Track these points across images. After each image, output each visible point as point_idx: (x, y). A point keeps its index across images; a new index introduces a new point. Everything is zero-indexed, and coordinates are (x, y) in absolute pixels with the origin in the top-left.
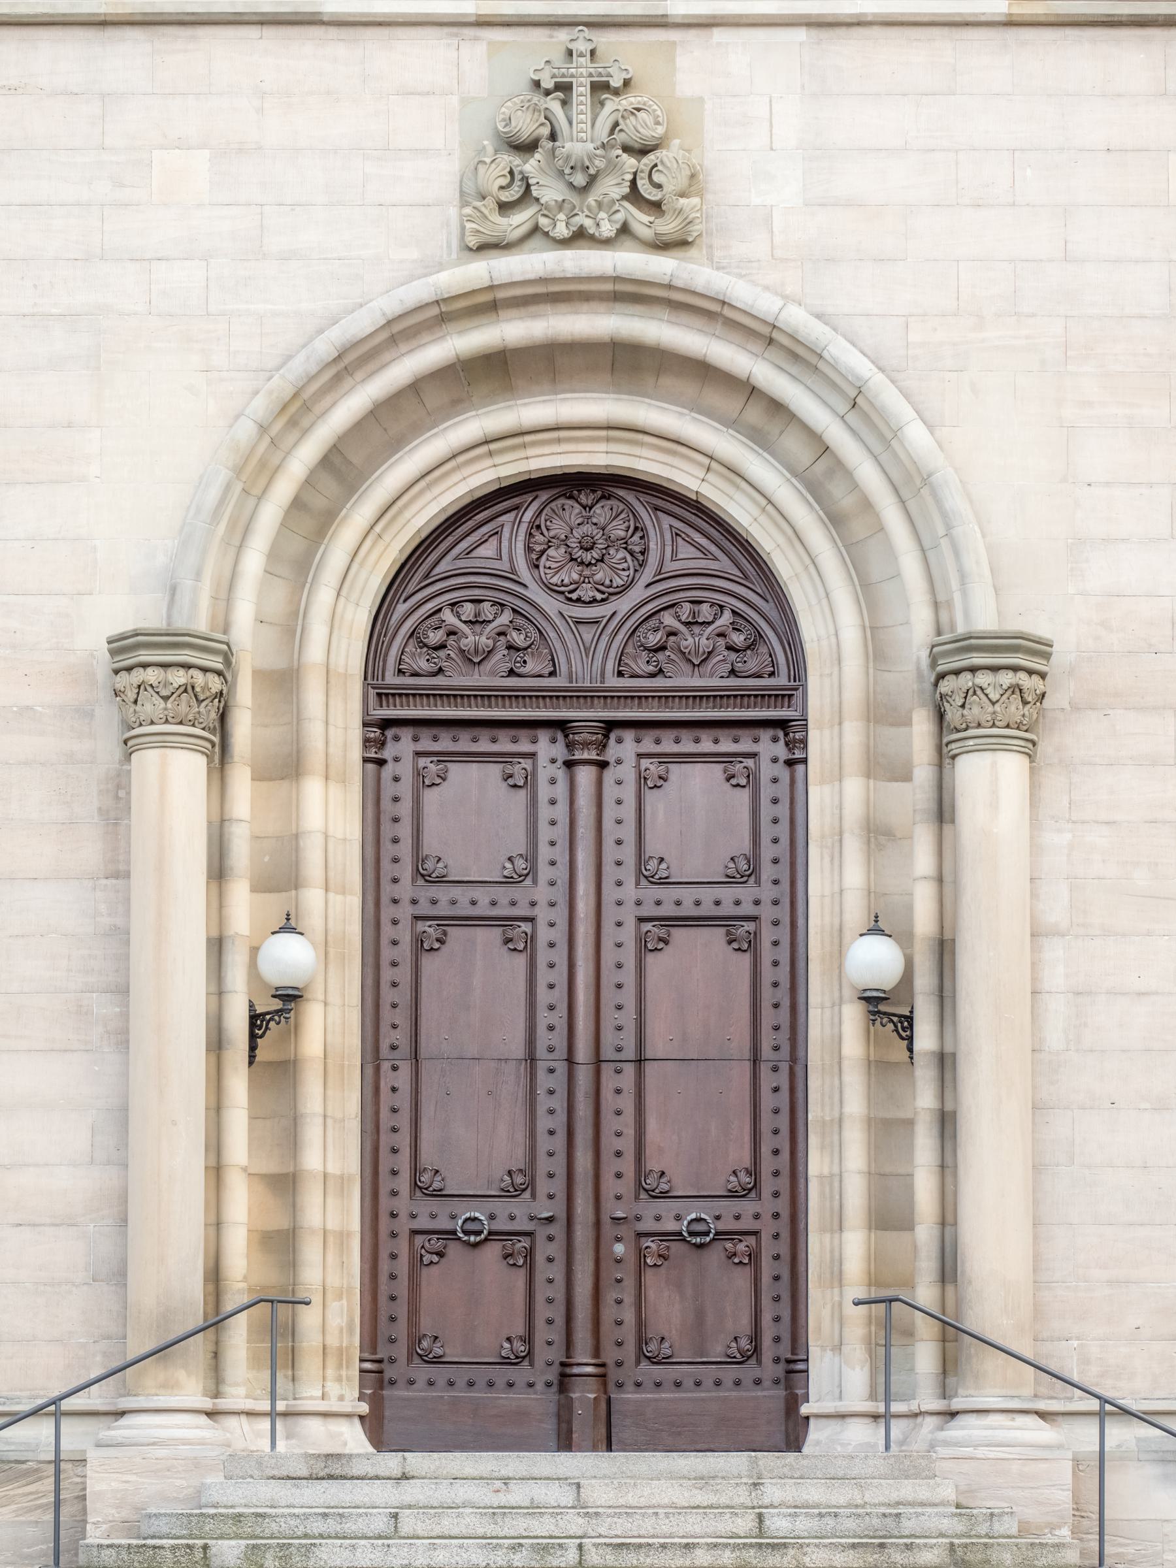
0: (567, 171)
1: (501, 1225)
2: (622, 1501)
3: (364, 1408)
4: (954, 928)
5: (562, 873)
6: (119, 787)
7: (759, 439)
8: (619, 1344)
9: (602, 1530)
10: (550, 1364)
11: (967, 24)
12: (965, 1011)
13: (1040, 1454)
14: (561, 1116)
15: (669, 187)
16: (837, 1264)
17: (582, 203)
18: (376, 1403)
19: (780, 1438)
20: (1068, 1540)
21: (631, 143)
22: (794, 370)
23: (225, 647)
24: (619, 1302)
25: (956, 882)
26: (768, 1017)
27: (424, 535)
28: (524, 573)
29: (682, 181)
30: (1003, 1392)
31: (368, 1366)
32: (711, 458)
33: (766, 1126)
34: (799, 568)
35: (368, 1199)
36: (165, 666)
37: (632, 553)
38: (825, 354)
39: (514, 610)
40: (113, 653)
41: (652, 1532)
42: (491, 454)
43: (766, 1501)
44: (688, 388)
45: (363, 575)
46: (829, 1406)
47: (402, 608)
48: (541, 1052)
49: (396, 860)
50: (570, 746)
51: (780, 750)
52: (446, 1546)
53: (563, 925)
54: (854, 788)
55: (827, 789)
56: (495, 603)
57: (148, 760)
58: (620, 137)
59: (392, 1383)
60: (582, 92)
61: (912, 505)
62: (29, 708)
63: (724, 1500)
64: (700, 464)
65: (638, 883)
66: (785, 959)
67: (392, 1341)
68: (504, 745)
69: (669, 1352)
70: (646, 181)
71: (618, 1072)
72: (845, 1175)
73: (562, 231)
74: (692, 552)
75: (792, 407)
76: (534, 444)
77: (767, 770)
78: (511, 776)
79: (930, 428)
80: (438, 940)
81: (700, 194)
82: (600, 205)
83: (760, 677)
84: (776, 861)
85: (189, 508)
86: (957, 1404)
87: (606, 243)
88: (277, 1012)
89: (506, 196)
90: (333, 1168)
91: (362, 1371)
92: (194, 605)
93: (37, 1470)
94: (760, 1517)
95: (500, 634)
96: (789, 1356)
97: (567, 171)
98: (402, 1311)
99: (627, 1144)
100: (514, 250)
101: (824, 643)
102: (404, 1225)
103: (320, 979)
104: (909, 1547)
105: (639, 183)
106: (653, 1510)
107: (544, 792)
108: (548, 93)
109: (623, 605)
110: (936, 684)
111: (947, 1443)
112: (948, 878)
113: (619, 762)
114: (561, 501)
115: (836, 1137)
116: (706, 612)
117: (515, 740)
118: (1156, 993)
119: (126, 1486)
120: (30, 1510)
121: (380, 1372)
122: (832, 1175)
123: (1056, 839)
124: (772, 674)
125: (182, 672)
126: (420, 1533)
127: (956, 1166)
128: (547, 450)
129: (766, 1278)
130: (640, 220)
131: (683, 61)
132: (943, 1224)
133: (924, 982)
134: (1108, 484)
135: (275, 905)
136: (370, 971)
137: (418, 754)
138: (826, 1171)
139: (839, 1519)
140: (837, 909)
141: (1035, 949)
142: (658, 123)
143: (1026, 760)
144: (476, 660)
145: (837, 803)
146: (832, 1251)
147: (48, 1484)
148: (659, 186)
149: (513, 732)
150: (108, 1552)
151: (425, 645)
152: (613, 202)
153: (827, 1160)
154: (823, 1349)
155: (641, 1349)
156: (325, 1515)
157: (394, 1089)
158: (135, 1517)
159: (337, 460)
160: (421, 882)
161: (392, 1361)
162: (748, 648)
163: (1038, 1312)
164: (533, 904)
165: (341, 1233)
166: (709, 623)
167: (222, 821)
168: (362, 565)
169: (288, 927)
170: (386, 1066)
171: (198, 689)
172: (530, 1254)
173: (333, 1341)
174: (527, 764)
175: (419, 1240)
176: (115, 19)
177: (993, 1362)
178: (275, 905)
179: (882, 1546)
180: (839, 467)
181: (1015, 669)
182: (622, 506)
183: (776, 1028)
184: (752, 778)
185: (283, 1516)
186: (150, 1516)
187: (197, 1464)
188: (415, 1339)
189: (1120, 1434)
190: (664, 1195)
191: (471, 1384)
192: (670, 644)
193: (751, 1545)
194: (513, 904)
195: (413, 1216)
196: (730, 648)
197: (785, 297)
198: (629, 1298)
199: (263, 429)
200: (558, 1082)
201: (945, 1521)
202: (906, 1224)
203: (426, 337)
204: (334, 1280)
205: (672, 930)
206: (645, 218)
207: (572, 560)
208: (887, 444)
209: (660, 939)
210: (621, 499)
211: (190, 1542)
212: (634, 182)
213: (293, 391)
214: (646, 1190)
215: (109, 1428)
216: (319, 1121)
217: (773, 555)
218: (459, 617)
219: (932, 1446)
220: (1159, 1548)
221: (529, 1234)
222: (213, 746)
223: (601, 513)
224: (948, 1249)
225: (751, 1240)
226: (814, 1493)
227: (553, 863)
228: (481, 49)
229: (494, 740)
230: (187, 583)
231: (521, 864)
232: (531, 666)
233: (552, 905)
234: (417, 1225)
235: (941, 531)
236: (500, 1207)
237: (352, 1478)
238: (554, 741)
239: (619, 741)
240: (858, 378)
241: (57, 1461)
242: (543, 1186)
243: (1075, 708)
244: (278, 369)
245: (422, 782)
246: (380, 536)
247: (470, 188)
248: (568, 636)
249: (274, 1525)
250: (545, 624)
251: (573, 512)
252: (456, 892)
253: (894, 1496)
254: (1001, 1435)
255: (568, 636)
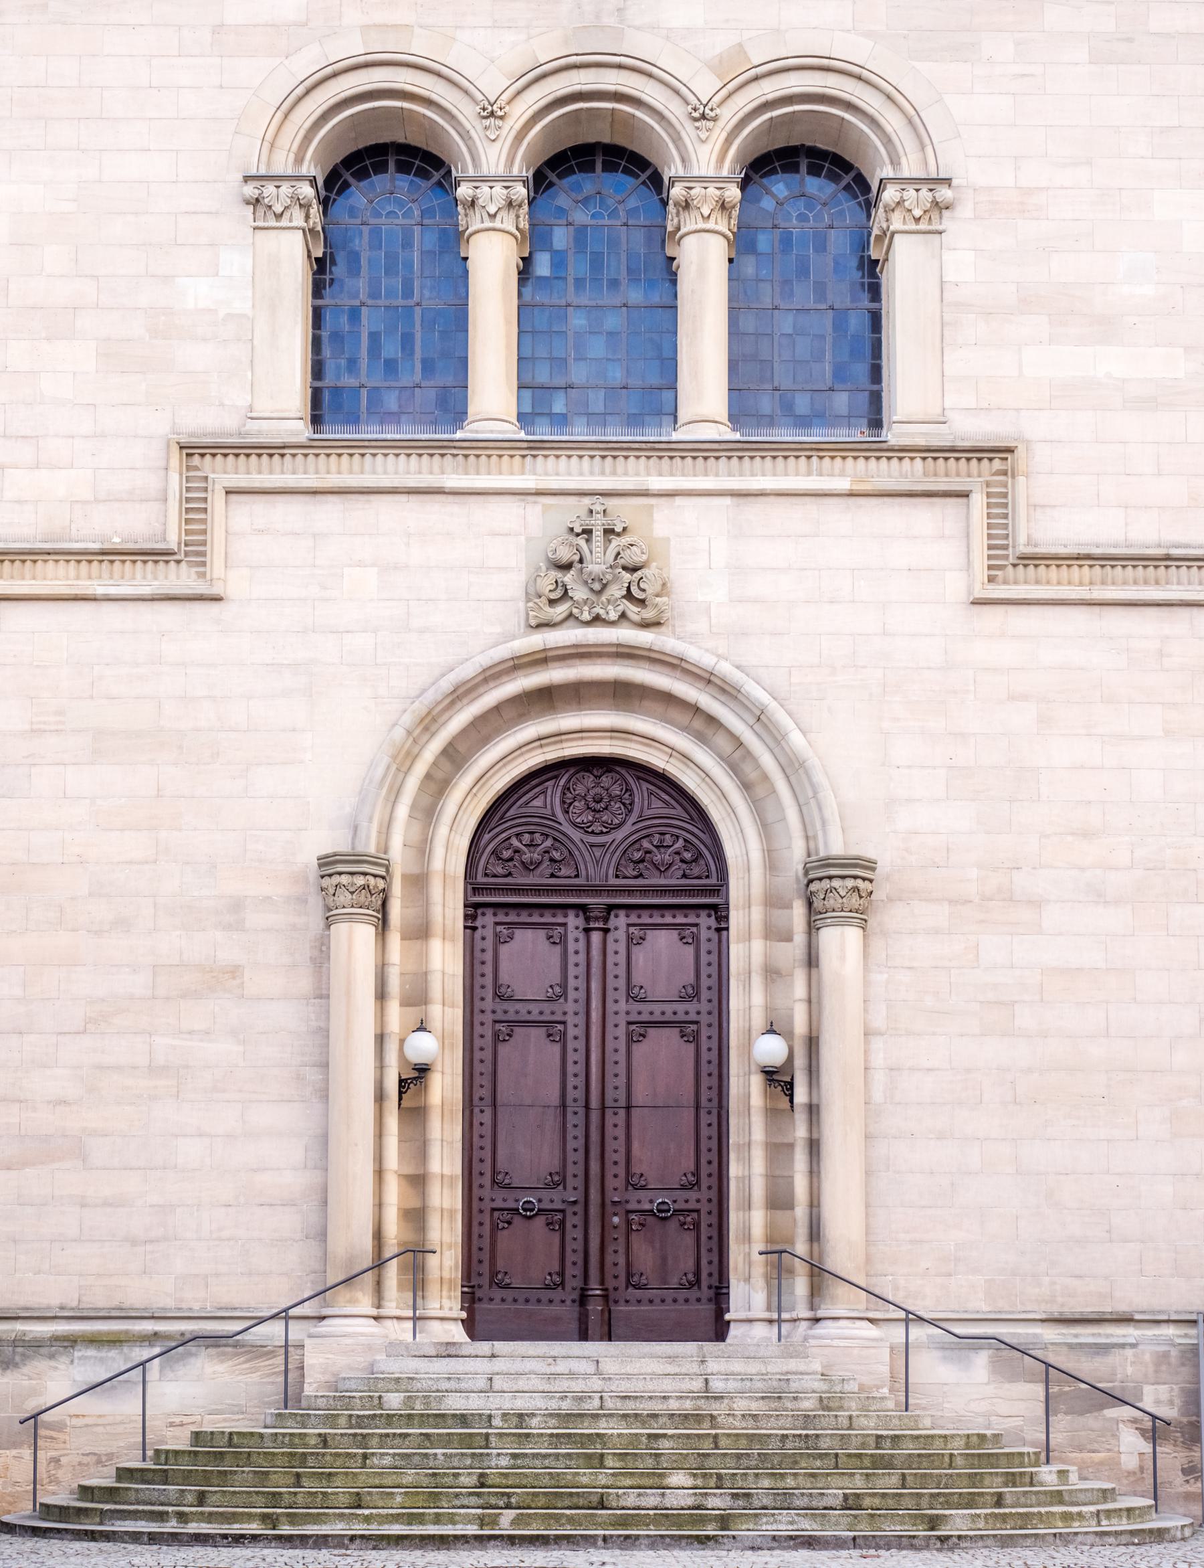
0: (590, 581)
1: (546, 1205)
2: (623, 1371)
3: (464, 1315)
4: (818, 1030)
5: (582, 995)
6: (322, 944)
7: (701, 738)
8: (616, 1277)
9: (613, 1388)
10: (574, 1289)
11: (826, 495)
12: (825, 1079)
13: (874, 1344)
14: (582, 1141)
15: (650, 591)
16: (747, 1230)
17: (598, 600)
18: (471, 1311)
19: (712, 1334)
20: (887, 1395)
21: (628, 565)
22: (723, 698)
23: (387, 862)
24: (616, 1252)
25: (819, 1003)
26: (705, 1082)
27: (500, 793)
28: (560, 816)
29: (658, 588)
30: (848, 1307)
31: (466, 1289)
32: (673, 749)
33: (703, 1148)
34: (725, 815)
35: (466, 1189)
36: (352, 874)
37: (624, 804)
38: (742, 690)
39: (554, 839)
40: (320, 866)
41: (642, 1389)
42: (541, 746)
43: (709, 1371)
44: (658, 707)
45: (465, 818)
46: (742, 1315)
47: (487, 837)
48: (569, 1102)
49: (483, 987)
50: (587, 919)
51: (712, 922)
52: (522, 1397)
53: (582, 1026)
54: (758, 946)
55: (741, 945)
56: (542, 834)
57: (341, 930)
58: (620, 561)
59: (480, 1300)
60: (598, 534)
61: (792, 779)
62: (269, 898)
63: (684, 1371)
64: (666, 753)
65: (627, 1001)
66: (715, 1046)
67: (480, 1275)
68: (548, 918)
69: (645, 1282)
70: (636, 587)
71: (616, 1114)
72: (752, 1177)
73: (586, 616)
74: (660, 804)
75: (722, 721)
76: (567, 740)
77: (704, 934)
78: (552, 937)
79: (804, 733)
80: (508, 1035)
81: (668, 595)
82: (609, 601)
83: (701, 878)
84: (709, 988)
85: (365, 779)
86: (820, 1314)
87: (612, 623)
88: (415, 1078)
89: (553, 596)
90: (447, 1171)
91: (463, 1293)
92: (368, 837)
93: (273, 1352)
94: (706, 1380)
95: (545, 852)
96: (717, 1284)
97: (590, 581)
98: (486, 1256)
99: (621, 1157)
100: (557, 628)
101: (740, 859)
102: (487, 1205)
103: (440, 1059)
104: (795, 1399)
105: (632, 588)
106: (643, 1376)
107: (571, 946)
108: (578, 535)
109: (619, 835)
110: (808, 885)
111: (814, 1337)
112: (814, 1000)
113: (616, 929)
114: (582, 774)
115: (747, 1154)
116: (668, 840)
117: (554, 916)
118: (938, 1069)
119: (327, 1361)
120: (269, 1375)
121: (473, 1293)
122: (744, 1177)
123: (879, 978)
124: (707, 877)
125: (362, 877)
126: (505, 1389)
127: (819, 1172)
128: (574, 743)
129: (703, 1238)
130: (633, 610)
131: (657, 516)
132: (811, 1206)
133: (800, 1062)
134: (909, 767)
135: (414, 1013)
136: (467, 1053)
137: (497, 924)
138: (740, 1174)
139: (753, 1382)
140: (747, 1017)
141: (867, 1042)
142: (643, 553)
143: (861, 930)
144: (532, 868)
145: (747, 954)
146: (744, 1222)
147: (280, 1360)
148: (644, 590)
149: (552, 911)
150: (321, 1400)
151: (501, 859)
152: (617, 600)
153: (741, 1167)
154: (739, 1280)
155: (629, 1280)
156: (449, 1379)
157: (481, 1124)
158: (333, 1380)
159: (451, 750)
160: (498, 1000)
161: (480, 1287)
162: (693, 861)
163: (868, 1259)
164: (565, 1013)
165: (451, 1211)
166: (670, 846)
167: (383, 965)
168: (464, 812)
169: (422, 1028)
170: (476, 1110)
171: (371, 887)
172: (563, 1223)
173: (446, 1275)
174: (560, 929)
175: (496, 1214)
176: (321, 490)
177: (842, 1290)
178: (414, 1013)
179: (779, 1398)
180: (749, 754)
181: (855, 877)
182: (618, 777)
183: (710, 1088)
184: (696, 939)
185: (424, 1379)
186: (344, 1379)
187: (370, 1348)
188: (494, 1273)
189: (918, 1333)
190: (643, 1188)
191: (527, 1301)
192: (647, 858)
193: (702, 1397)
194: (553, 1013)
195: (493, 1200)
196: (682, 861)
197: (718, 656)
198: (622, 1250)
199: (409, 733)
200: (580, 1119)
201: (816, 1383)
202: (789, 1205)
203: (505, 679)
204: (447, 1238)
205: (648, 1029)
206: (636, 609)
207: (588, 808)
208: (778, 743)
209: (641, 1035)
210: (618, 773)
211: (371, 1394)
212: (629, 588)
213: (427, 710)
214: (632, 1185)
215: (316, 1326)
216: (439, 1143)
217: (709, 807)
218: (521, 842)
219: (806, 1339)
220: (941, 1400)
221: (563, 1211)
222: (379, 919)
223: (606, 780)
224: (814, 1222)
225: (695, 1215)
226: (737, 1366)
227: (577, 989)
228: (538, 509)
229: (542, 916)
230: (364, 824)
231: (558, 990)
232: (564, 872)
233: (576, 1014)
234: (495, 1205)
235: (810, 794)
236: (546, 1195)
237: (462, 1357)
238: (577, 916)
239: (616, 916)
240: (763, 705)
241: (286, 1346)
242: (571, 1182)
243: (890, 900)
244: (418, 697)
245: (499, 941)
246: (475, 795)
247: (531, 590)
248: (586, 854)
249: (419, 1384)
250: (572, 846)
251: (589, 780)
252: (519, 1006)
253: (785, 1369)
254: (847, 1332)
255: (586, 854)
